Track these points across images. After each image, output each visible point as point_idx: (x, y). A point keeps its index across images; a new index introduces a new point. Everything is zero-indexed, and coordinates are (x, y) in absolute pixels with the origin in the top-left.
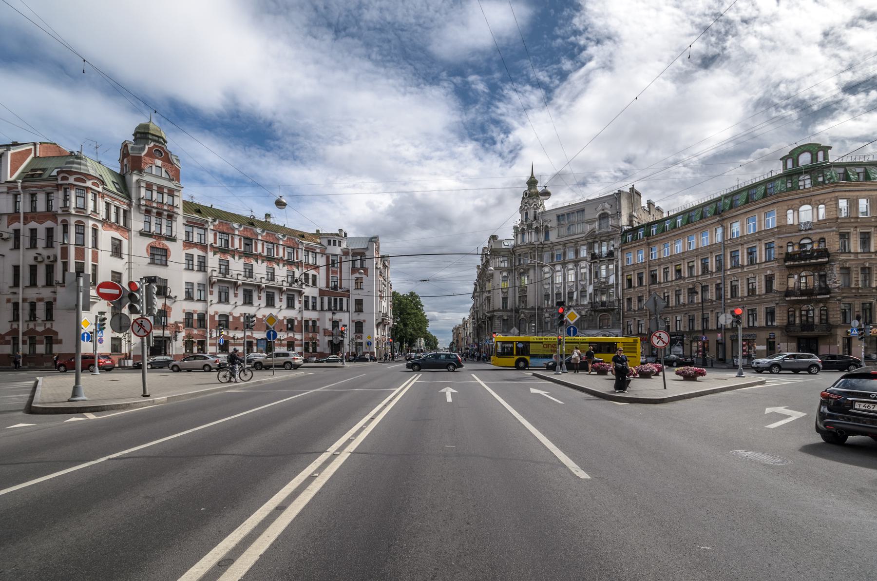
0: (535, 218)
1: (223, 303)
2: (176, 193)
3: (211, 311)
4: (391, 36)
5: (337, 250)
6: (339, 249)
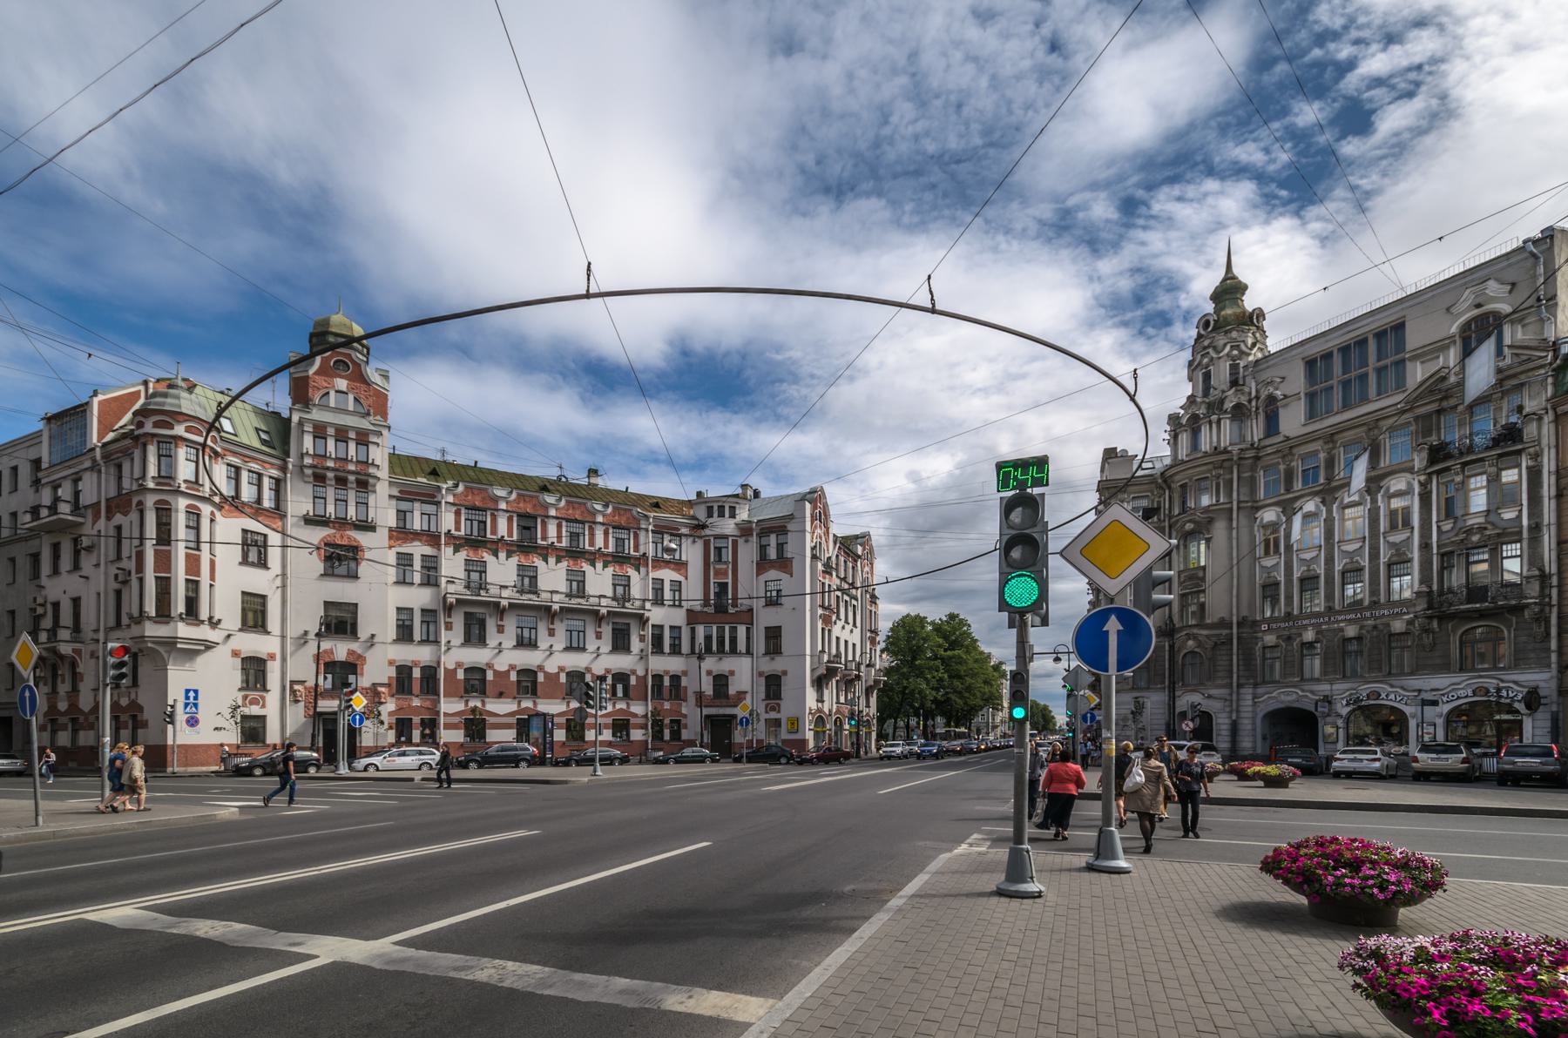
0: (1234, 383)
1: (474, 645)
2: (373, 439)
3: (448, 661)
4: (937, 175)
5: (728, 526)
6: (732, 521)
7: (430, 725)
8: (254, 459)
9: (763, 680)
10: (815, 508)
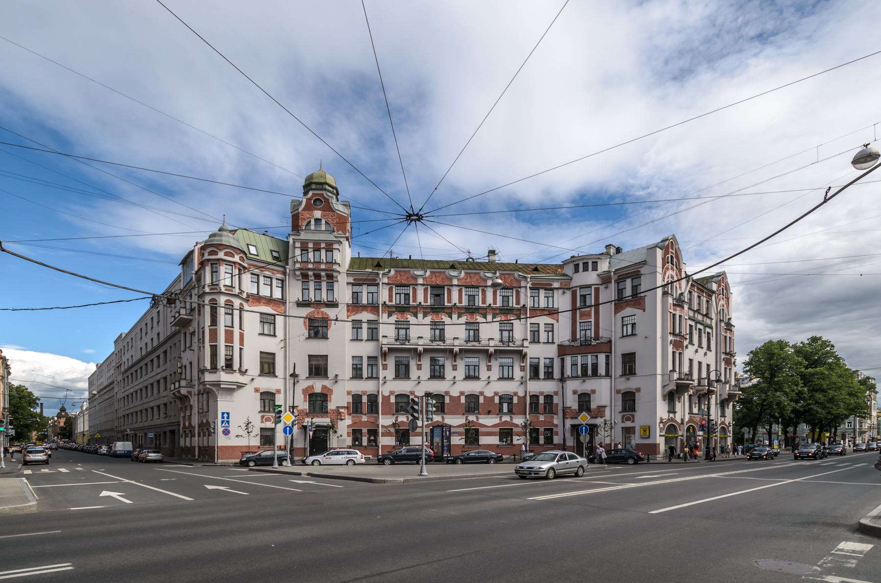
1: (402, 379)
3: (385, 390)
5: (591, 277)
6: (595, 273)
7: (373, 433)
8: (268, 269)
9: (620, 397)
10: (666, 252)
